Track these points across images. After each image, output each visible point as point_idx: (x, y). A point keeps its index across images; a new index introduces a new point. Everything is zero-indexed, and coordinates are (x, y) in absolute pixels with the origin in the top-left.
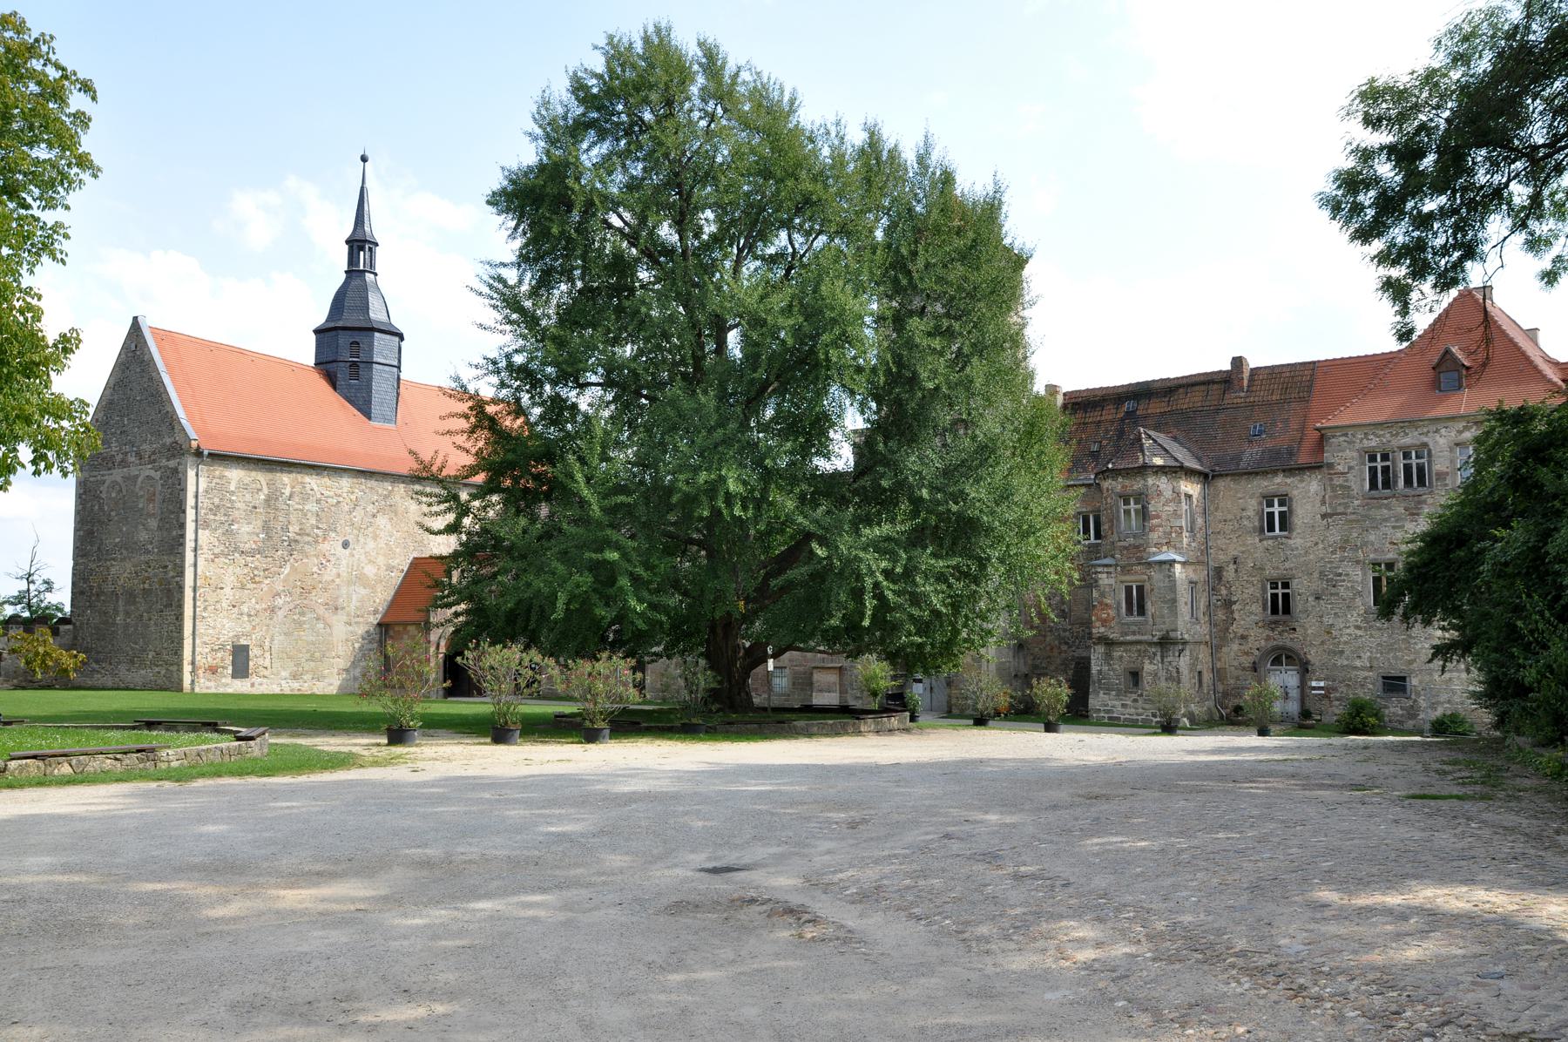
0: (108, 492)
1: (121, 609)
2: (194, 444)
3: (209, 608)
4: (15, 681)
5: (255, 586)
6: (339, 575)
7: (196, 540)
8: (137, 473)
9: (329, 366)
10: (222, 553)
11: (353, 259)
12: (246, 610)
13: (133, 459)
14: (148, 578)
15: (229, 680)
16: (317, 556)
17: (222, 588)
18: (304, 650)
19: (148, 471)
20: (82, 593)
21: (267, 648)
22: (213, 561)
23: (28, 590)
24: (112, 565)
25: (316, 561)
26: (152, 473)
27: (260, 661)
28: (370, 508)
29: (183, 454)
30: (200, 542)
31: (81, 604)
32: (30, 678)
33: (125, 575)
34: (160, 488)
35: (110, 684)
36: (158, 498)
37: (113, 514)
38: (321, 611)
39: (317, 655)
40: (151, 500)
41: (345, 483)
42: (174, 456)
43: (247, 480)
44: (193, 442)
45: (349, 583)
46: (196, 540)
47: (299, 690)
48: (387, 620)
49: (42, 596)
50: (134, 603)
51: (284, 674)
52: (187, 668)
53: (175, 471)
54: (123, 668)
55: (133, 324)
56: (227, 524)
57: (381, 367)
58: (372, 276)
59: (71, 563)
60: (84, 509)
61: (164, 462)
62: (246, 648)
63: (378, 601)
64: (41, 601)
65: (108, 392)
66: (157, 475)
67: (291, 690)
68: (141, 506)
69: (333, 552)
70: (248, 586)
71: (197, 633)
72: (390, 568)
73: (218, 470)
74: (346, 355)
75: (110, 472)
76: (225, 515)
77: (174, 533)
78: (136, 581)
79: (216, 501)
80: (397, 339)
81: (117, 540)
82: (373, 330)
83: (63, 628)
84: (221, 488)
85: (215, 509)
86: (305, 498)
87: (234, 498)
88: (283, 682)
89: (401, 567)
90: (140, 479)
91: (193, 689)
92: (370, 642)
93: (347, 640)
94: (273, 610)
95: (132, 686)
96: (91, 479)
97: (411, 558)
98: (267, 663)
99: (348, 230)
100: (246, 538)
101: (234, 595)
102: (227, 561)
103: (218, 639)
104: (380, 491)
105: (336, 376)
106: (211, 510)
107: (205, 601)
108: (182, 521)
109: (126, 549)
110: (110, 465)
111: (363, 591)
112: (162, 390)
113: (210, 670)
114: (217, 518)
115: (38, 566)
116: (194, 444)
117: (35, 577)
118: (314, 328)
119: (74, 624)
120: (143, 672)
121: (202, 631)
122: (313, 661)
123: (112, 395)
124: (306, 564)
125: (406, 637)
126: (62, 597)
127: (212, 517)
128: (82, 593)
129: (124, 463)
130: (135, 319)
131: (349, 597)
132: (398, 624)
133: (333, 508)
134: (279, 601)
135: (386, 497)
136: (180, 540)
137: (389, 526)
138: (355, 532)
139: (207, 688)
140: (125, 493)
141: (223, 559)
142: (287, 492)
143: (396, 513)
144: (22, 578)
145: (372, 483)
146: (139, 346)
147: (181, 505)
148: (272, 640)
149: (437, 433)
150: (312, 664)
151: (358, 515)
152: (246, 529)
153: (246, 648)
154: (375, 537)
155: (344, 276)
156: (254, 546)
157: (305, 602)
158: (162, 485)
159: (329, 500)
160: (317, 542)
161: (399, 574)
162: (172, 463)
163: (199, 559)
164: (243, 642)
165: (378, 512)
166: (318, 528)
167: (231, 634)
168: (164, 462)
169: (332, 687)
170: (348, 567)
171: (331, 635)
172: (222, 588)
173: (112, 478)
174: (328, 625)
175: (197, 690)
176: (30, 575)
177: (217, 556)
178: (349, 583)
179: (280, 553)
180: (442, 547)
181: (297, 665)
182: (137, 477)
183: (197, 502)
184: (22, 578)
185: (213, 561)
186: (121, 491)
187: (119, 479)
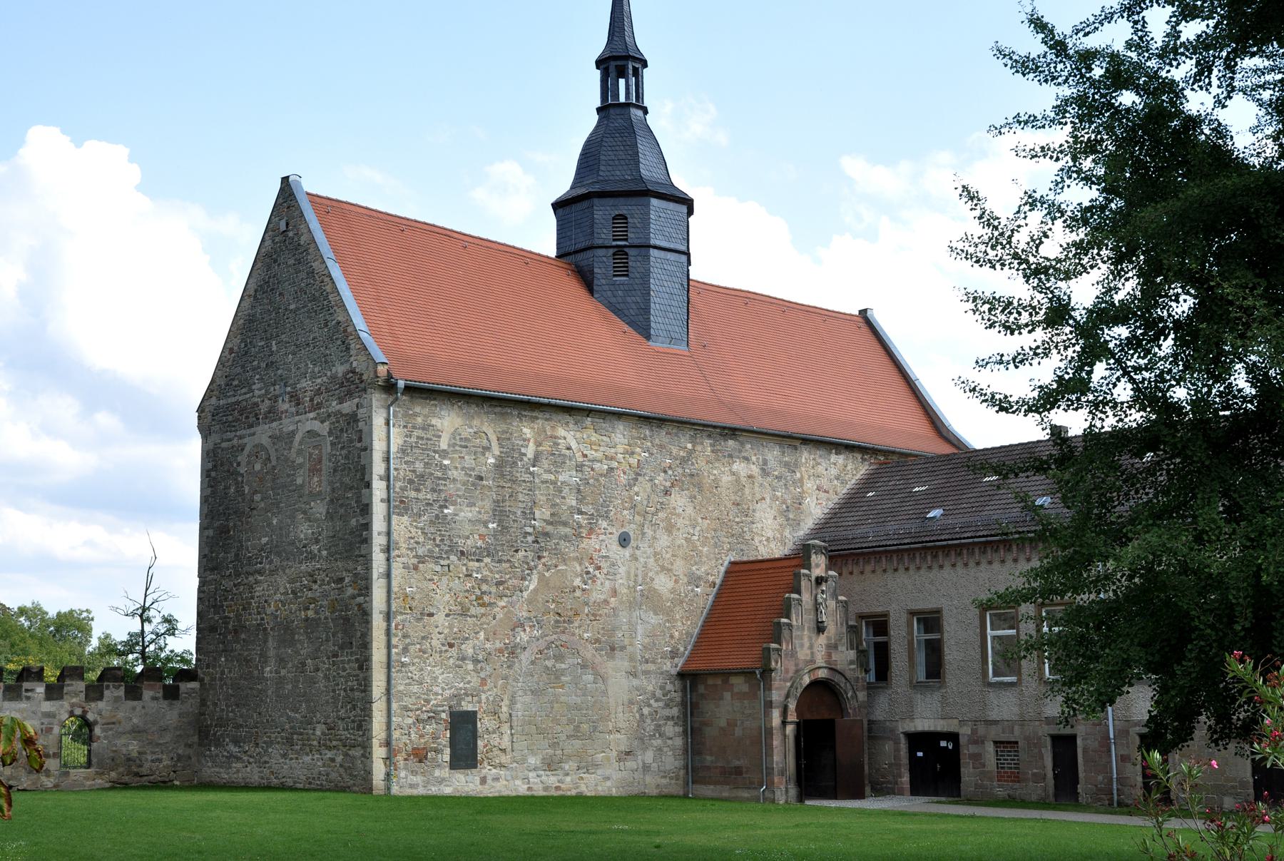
0: (248, 463)
1: (271, 653)
2: (382, 370)
3: (412, 648)
4: (113, 774)
5: (483, 610)
6: (614, 592)
7: (389, 534)
8: (291, 428)
9: (580, 257)
10: (430, 555)
11: (607, 89)
12: (470, 651)
13: (286, 406)
14: (314, 600)
15: (445, 772)
16: (580, 560)
17: (431, 615)
18: (564, 720)
19: (310, 423)
20: (213, 629)
21: (504, 716)
22: (416, 568)
23: (143, 631)
24: (257, 582)
25: (578, 568)
26: (316, 426)
27: (495, 740)
28: (660, 478)
29: (365, 390)
30: (395, 536)
31: (212, 647)
32: (134, 769)
33: (278, 596)
34: (329, 448)
35: (255, 779)
36: (326, 465)
37: (257, 497)
38: (589, 652)
39: (585, 727)
40: (315, 470)
41: (620, 435)
42: (350, 394)
43: (467, 432)
44: (380, 368)
45: (632, 605)
46: (389, 534)
47: (557, 788)
48: (693, 667)
49: (162, 642)
50: (292, 643)
51: (532, 761)
52: (378, 752)
53: (353, 418)
54: (275, 751)
55: (281, 190)
56: (436, 506)
57: (662, 254)
58: (640, 113)
59: (195, 582)
60: (213, 493)
61: (335, 406)
62: (471, 717)
63: (677, 634)
64: (161, 649)
65: (246, 304)
66: (323, 429)
67: (546, 789)
68: (299, 481)
69: (604, 553)
70: (473, 611)
71: (393, 691)
72: (694, 580)
73: (421, 410)
74: (605, 235)
75: (252, 430)
76: (434, 490)
77: (353, 522)
78: (294, 607)
79: (419, 466)
80: (684, 209)
81: (264, 540)
82: (647, 193)
83: (186, 686)
84: (421, 445)
85: (417, 481)
86: (559, 461)
87: (446, 462)
88: (531, 775)
89: (711, 579)
90: (298, 438)
91: (389, 789)
92: (667, 705)
93: (631, 702)
94: (513, 651)
95: (290, 782)
96: (224, 445)
97: (726, 563)
98: (506, 743)
99: (598, 43)
100: (467, 529)
101: (451, 627)
102: (438, 568)
103: (427, 701)
104: (675, 451)
105: (592, 272)
106: (411, 482)
107: (405, 636)
108: (365, 501)
109: (278, 554)
110: (252, 419)
111: (654, 619)
112: (328, 288)
113: (416, 755)
114: (421, 496)
115: (155, 596)
116: (382, 370)
117: (152, 613)
118: (553, 199)
119: (202, 681)
120: (307, 759)
121: (401, 688)
122: (577, 738)
123: (253, 307)
124: (563, 573)
125: (727, 695)
126: (184, 643)
127: (413, 494)
128: (213, 629)
129: (273, 415)
130: (285, 180)
131: (633, 631)
132: (715, 674)
133: (602, 479)
134: (522, 637)
135: (684, 461)
136: (362, 534)
137: (690, 510)
138: (638, 518)
139: (412, 786)
140: (274, 463)
141: (432, 566)
142: (530, 451)
143: (700, 487)
144: (133, 614)
145: (662, 436)
146: (292, 223)
147: (363, 475)
148: (513, 702)
149: (1001, 53)
150: (577, 743)
151: (641, 491)
152: (467, 513)
153: (471, 717)
154: (670, 528)
155: (594, 119)
156: (480, 543)
157: (564, 637)
158: (333, 444)
159: (597, 466)
160: (579, 536)
161: (709, 590)
162: (347, 407)
163: (394, 565)
164: (467, 706)
165: (673, 485)
166: (580, 513)
167: (447, 693)
168: (335, 406)
169: (608, 783)
170: (628, 578)
171: (605, 693)
172: (431, 615)
173: (256, 440)
174: (600, 677)
175: (395, 790)
176: (144, 609)
177: (422, 560)
178: (632, 605)
179: (521, 554)
180: (772, 545)
181: (554, 745)
182: (293, 433)
183: (388, 469)
184: (133, 614)
185: (416, 568)
186: (269, 459)
187: (265, 441)
